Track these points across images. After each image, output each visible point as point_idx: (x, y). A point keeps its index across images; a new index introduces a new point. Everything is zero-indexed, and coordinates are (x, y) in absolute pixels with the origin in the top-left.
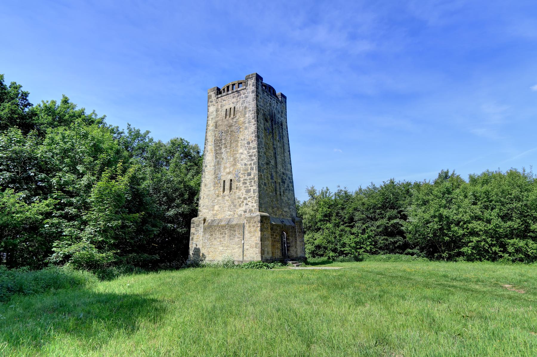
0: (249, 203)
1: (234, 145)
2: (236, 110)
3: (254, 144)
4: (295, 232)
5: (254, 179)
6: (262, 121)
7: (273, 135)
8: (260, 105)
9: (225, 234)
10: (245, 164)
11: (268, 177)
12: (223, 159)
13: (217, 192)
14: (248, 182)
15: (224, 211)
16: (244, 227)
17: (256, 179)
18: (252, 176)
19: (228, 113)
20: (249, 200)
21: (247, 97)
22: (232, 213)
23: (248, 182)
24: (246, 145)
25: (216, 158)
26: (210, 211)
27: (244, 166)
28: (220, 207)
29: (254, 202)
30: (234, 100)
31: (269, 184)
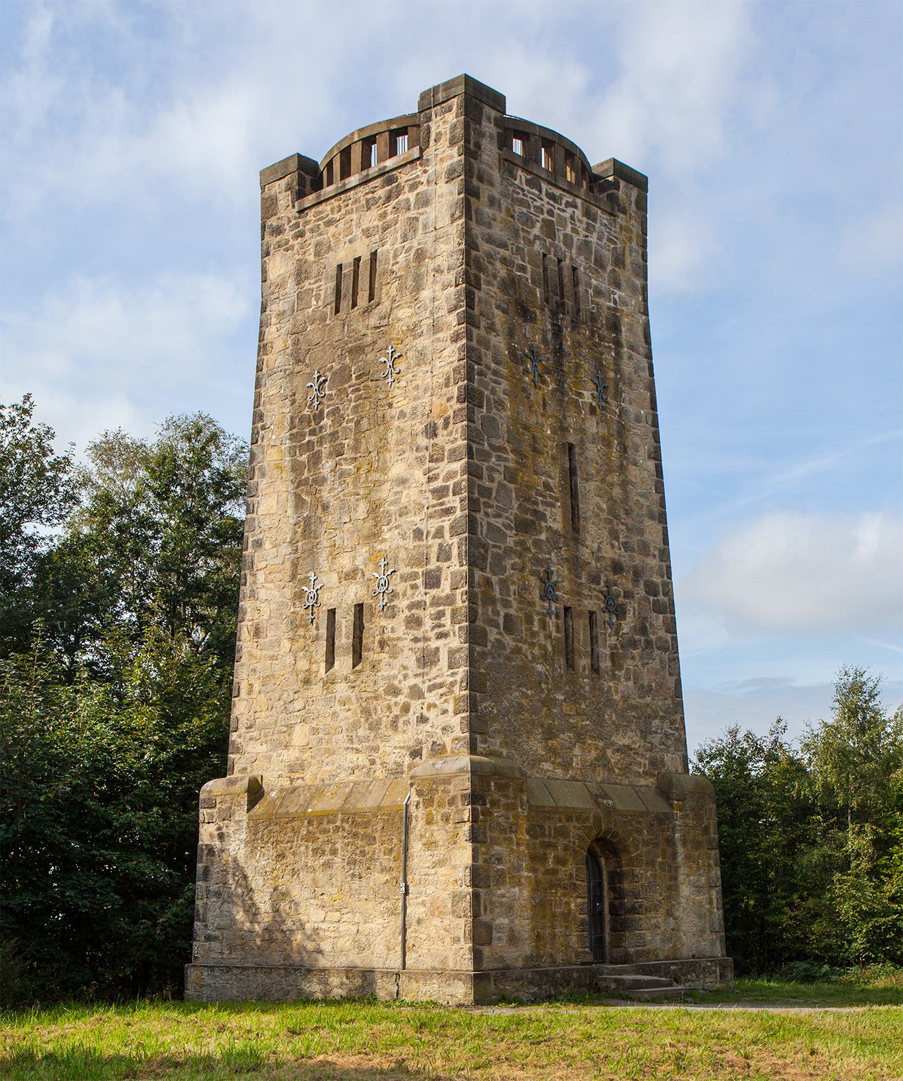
0: (431, 715)
1: (372, 439)
2: (379, 269)
3: (454, 438)
4: (670, 842)
5: (450, 600)
6: (499, 318)
7: (560, 382)
8: (490, 240)
9: (334, 852)
10: (418, 534)
11: (524, 588)
12: (325, 508)
13: (303, 665)
14: (427, 616)
15: (330, 752)
16: (408, 818)
17: (461, 603)
18: (445, 587)
19: (347, 284)
20: (431, 697)
21: (424, 201)
22: (362, 759)
23: (427, 616)
24: (423, 441)
25: (299, 503)
26: (275, 748)
27: (411, 543)
28: (315, 731)
29: (451, 707)
30: (371, 219)
31: (529, 620)
